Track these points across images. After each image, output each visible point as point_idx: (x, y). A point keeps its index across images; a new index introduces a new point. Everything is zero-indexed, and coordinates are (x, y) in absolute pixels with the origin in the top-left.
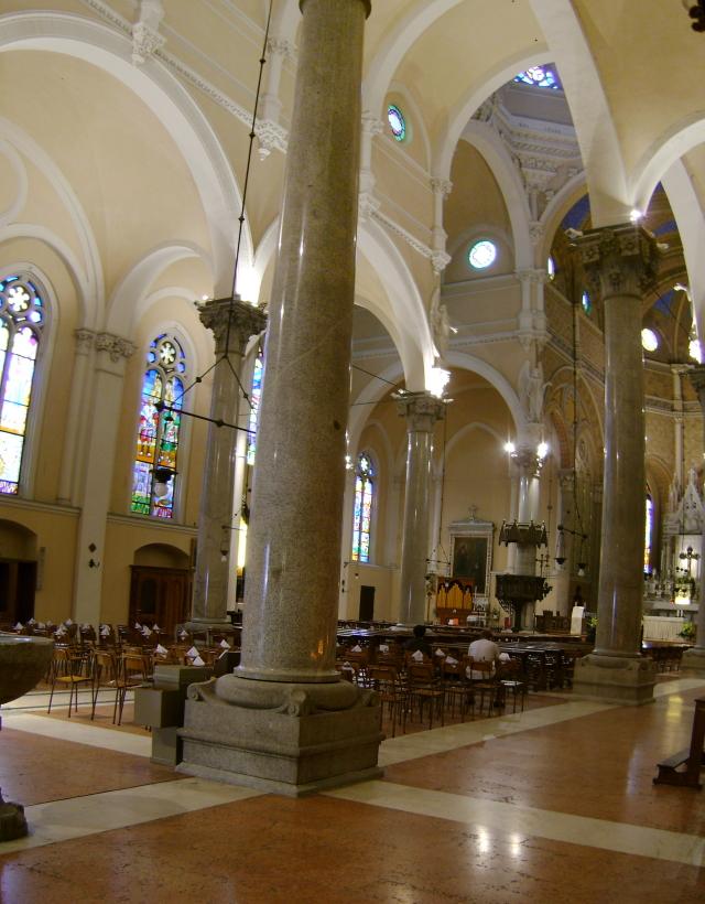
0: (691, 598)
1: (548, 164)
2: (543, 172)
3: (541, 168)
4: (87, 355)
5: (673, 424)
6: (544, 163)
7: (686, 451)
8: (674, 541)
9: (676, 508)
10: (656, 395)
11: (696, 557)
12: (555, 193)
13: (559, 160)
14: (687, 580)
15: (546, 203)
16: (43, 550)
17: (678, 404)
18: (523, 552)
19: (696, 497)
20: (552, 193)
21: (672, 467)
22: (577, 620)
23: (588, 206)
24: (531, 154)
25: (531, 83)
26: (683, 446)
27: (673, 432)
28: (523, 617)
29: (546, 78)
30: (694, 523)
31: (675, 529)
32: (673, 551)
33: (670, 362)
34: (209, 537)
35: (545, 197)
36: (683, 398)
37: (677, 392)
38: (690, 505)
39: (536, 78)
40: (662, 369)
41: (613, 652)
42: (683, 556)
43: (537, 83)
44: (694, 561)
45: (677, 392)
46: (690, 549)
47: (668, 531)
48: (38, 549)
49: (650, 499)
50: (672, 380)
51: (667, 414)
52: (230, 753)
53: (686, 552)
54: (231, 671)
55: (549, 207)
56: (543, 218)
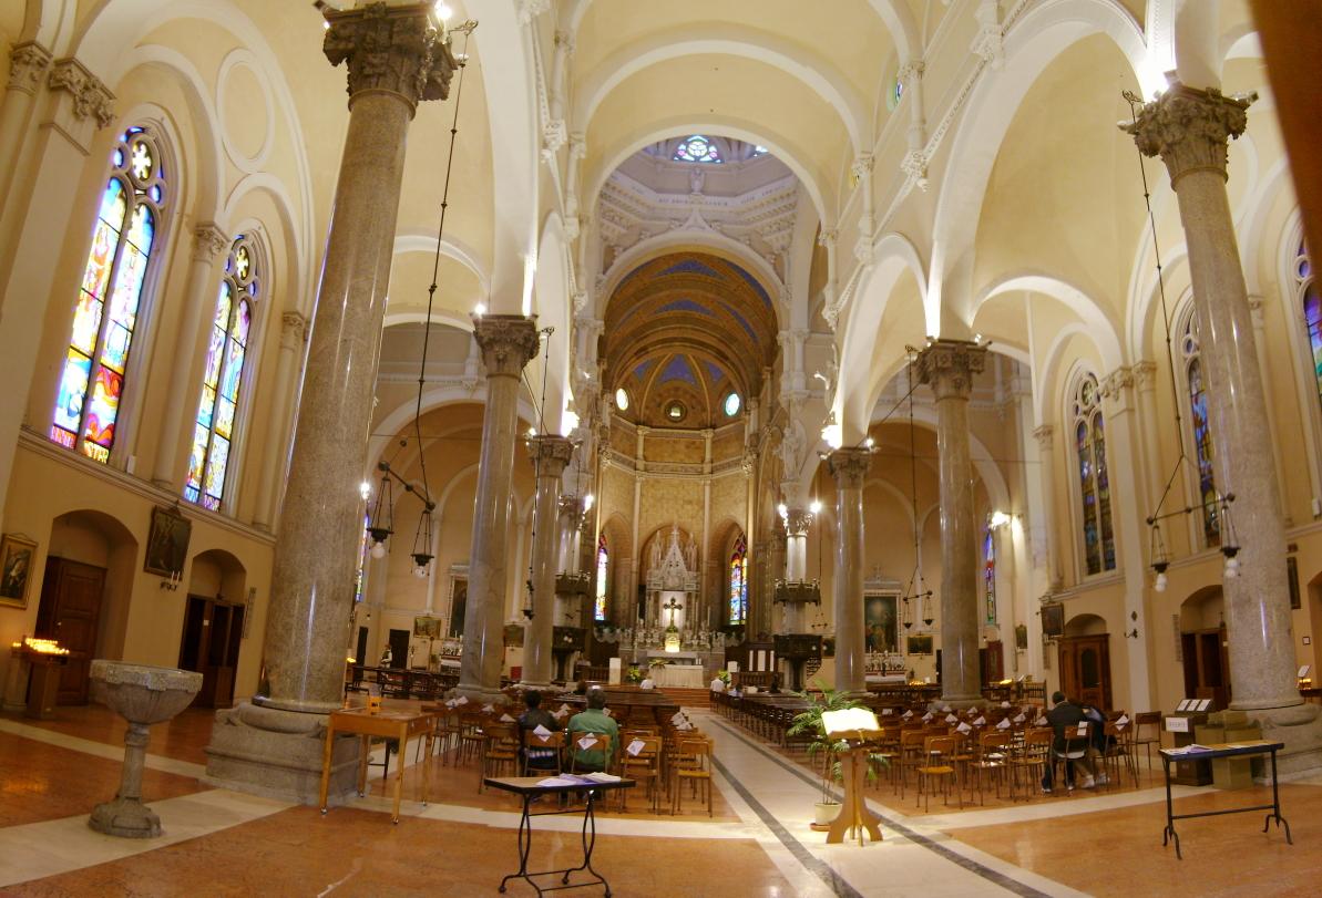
0: (680, 647)
1: (624, 221)
2: (616, 226)
3: (616, 223)
4: (294, 351)
5: (634, 482)
6: (621, 218)
7: (644, 510)
8: (657, 594)
9: (658, 567)
10: (623, 453)
11: (680, 607)
12: (625, 250)
13: (634, 219)
14: (672, 629)
15: (614, 257)
16: (253, 591)
17: (641, 464)
18: (565, 602)
19: (679, 557)
20: (621, 249)
21: (631, 524)
22: (615, 670)
23: (1006, 357)
24: (612, 206)
25: (693, 159)
26: (641, 503)
27: (634, 489)
28: (566, 669)
29: (708, 153)
30: (677, 580)
31: (659, 585)
32: (657, 601)
33: (637, 423)
34: (491, 590)
35: (614, 251)
36: (645, 458)
37: (640, 452)
38: (674, 563)
39: (698, 154)
40: (630, 428)
41: (968, 696)
42: (666, 606)
43: (697, 159)
44: (677, 611)
45: (640, 452)
46: (673, 600)
47: (652, 587)
48: (247, 588)
49: (606, 552)
50: (636, 440)
51: (630, 471)
52: (1301, 758)
53: (669, 602)
54: (1227, 707)
55: (617, 262)
56: (608, 273)
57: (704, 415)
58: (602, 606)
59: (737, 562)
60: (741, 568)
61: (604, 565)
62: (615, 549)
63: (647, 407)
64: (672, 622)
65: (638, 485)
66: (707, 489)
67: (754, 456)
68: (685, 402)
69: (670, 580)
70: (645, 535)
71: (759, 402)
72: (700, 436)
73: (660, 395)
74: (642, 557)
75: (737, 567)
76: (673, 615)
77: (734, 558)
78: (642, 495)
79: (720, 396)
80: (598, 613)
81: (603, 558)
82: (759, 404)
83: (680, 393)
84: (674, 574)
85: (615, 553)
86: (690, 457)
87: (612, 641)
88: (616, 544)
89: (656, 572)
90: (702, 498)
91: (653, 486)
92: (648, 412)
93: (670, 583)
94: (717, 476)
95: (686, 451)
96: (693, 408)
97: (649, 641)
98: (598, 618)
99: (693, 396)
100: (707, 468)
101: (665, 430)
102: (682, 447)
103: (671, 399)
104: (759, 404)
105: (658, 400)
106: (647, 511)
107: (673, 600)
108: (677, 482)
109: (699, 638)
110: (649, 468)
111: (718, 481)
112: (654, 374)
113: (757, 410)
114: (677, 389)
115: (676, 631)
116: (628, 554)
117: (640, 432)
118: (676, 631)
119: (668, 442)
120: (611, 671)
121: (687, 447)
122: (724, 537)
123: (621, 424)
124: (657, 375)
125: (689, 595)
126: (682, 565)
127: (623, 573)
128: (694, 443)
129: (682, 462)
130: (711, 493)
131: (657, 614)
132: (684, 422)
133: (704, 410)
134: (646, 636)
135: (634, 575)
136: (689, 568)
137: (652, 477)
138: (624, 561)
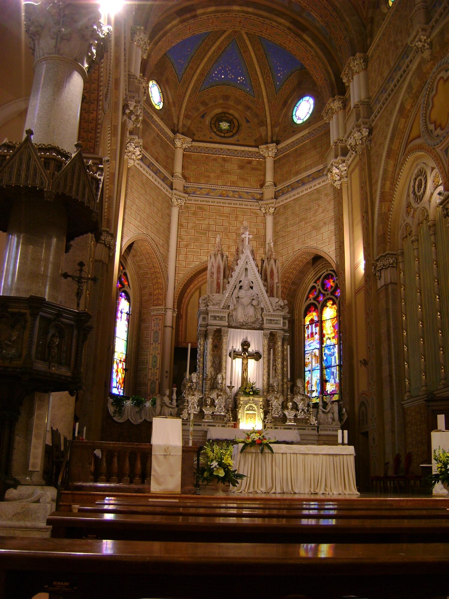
5: (170, 206)
7: (183, 243)
8: (218, 335)
11: (257, 356)
17: (179, 183)
19: (254, 275)
21: (166, 259)
22: (167, 451)
27: (169, 216)
30: (251, 311)
31: (221, 318)
32: (217, 347)
37: (178, 169)
38: (245, 283)
42: (235, 355)
44: (252, 363)
45: (178, 169)
46: (245, 344)
50: (174, 154)
51: (164, 188)
57: (262, 130)
58: (121, 375)
59: (314, 315)
60: (320, 323)
61: (125, 316)
62: (141, 297)
63: (187, 116)
64: (244, 379)
65: (175, 212)
66: (269, 220)
67: (365, 132)
68: (236, 115)
69: (240, 311)
70: (184, 275)
71: (345, 104)
72: (258, 154)
73: (204, 103)
74: (179, 308)
75: (312, 322)
76: (245, 369)
77: (307, 311)
78: (180, 225)
79: (285, 103)
80: (114, 384)
81: (124, 305)
82: (367, 66)
83: (231, 103)
84: (245, 301)
85: (141, 303)
86: (245, 180)
87: (137, 420)
88: (142, 289)
89: (216, 297)
90: (262, 232)
91: (194, 214)
92: (189, 122)
93: (240, 316)
94: (284, 200)
95: (238, 171)
96: (248, 121)
97: (207, 411)
98: (115, 391)
99: (248, 108)
100: (269, 192)
101: (212, 145)
102: (233, 167)
103: (218, 111)
104: (367, 66)
105: (202, 109)
106: (187, 246)
107: (245, 344)
108: (227, 210)
109: (295, 407)
110: (189, 190)
111: (285, 207)
112: (198, 71)
113: (362, 74)
114: (226, 98)
115: (256, 393)
116: (161, 300)
117: (178, 143)
118: (256, 393)
119: (215, 159)
120: (156, 453)
121: (241, 167)
122: (293, 283)
123: (154, 122)
124: (202, 74)
125: (272, 338)
126: (260, 286)
127: (153, 326)
128: (250, 162)
129: (234, 184)
130: (275, 224)
131: (218, 367)
132: (236, 137)
133: (263, 123)
134: (202, 403)
135: (169, 330)
136: (271, 293)
137: (193, 201)
138: (154, 311)
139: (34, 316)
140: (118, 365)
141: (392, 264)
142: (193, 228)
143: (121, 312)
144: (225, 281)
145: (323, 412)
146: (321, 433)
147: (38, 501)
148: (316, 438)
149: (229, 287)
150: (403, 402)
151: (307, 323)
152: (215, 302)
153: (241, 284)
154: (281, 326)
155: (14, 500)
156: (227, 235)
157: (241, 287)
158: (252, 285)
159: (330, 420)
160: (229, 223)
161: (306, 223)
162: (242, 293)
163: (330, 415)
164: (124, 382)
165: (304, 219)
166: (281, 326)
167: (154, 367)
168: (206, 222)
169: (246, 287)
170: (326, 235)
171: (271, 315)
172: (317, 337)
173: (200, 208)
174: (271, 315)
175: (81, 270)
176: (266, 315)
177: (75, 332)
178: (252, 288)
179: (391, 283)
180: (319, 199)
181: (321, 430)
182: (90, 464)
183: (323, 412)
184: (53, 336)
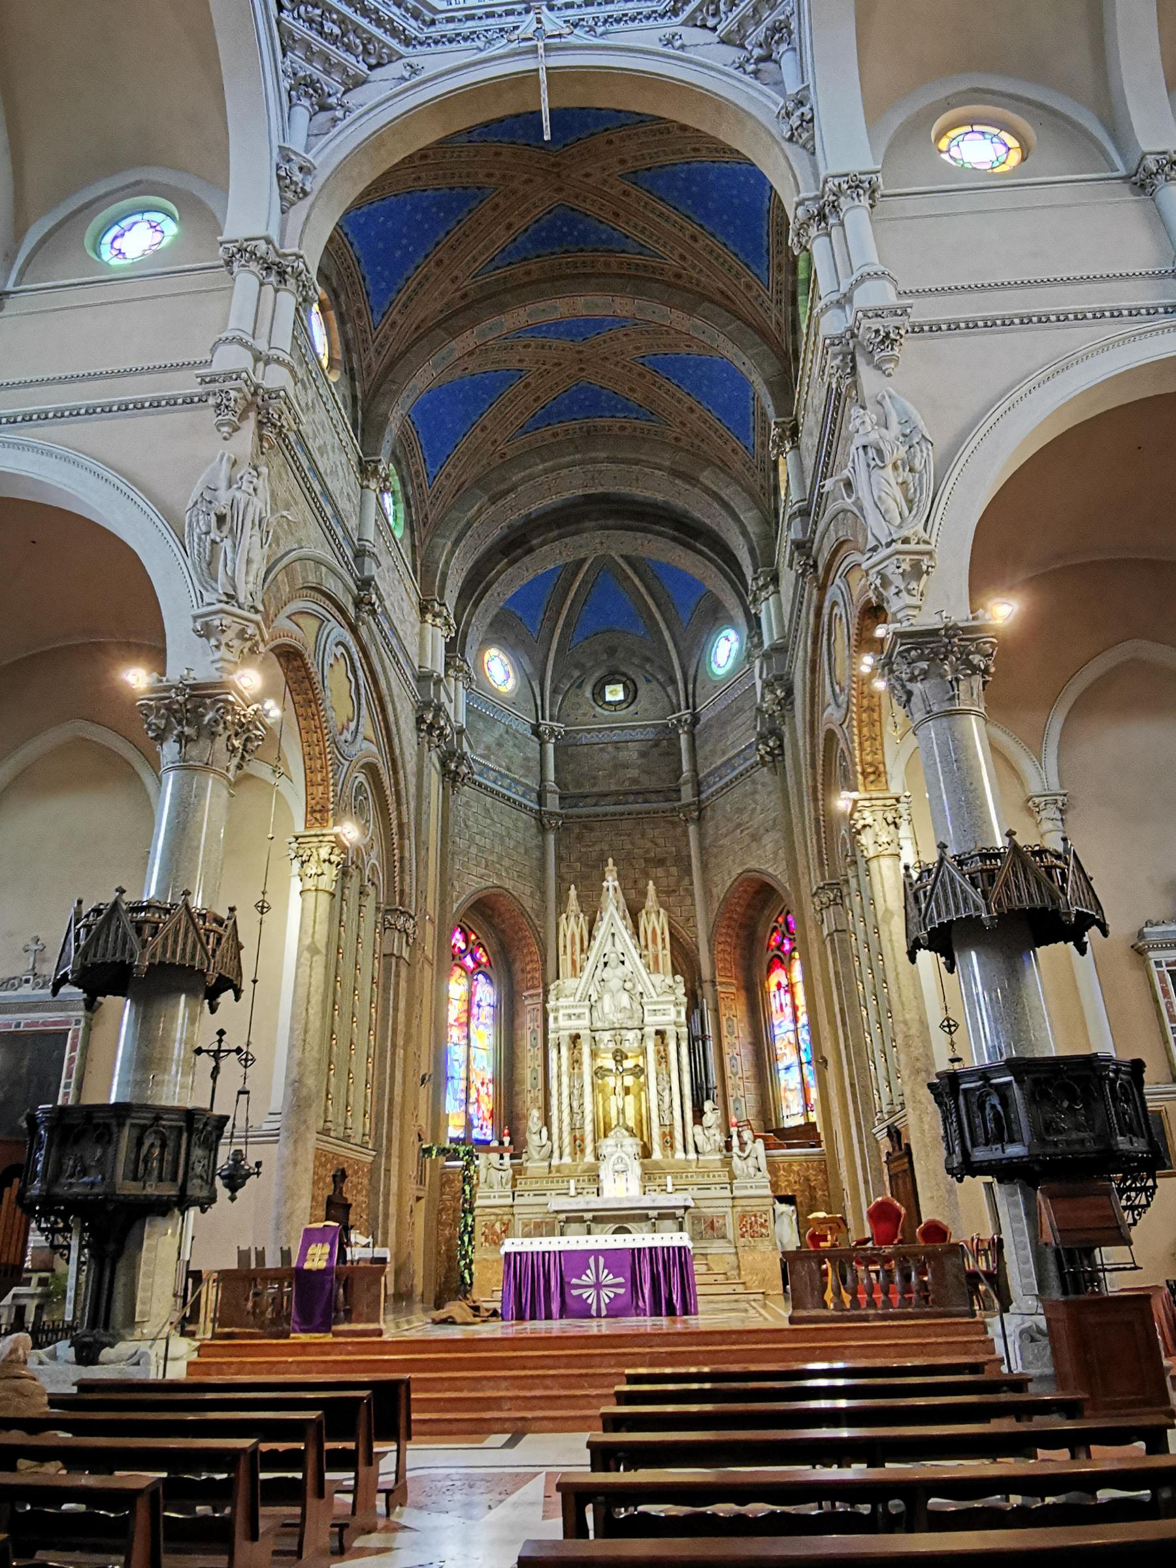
38: (613, 959)
84: (615, 984)
139: (121, 1125)
140: (478, 1091)
141: (834, 900)
142: (579, 860)
143: (479, 1006)
144: (584, 956)
145: (740, 1157)
146: (736, 1193)
147: (138, 1364)
148: (729, 1202)
149: (589, 966)
150: (874, 1131)
151: (773, 988)
152: (567, 992)
153: (606, 959)
154: (672, 1016)
155: (111, 1362)
156: (631, 864)
157: (606, 964)
158: (622, 958)
159: (752, 1171)
160: (632, 844)
161: (742, 831)
162: (607, 973)
163: (751, 1161)
164: (492, 1116)
165: (739, 825)
166: (672, 1016)
167: (534, 1087)
168: (597, 848)
169: (613, 961)
170: (770, 847)
171: (655, 1003)
172: (788, 1010)
173: (586, 827)
174: (655, 1003)
175: (220, 1041)
176: (648, 1003)
177: (185, 1136)
178: (623, 963)
179: (837, 931)
180: (755, 792)
181: (737, 1188)
182: (247, 1299)
183: (740, 1157)
184: (152, 1145)
